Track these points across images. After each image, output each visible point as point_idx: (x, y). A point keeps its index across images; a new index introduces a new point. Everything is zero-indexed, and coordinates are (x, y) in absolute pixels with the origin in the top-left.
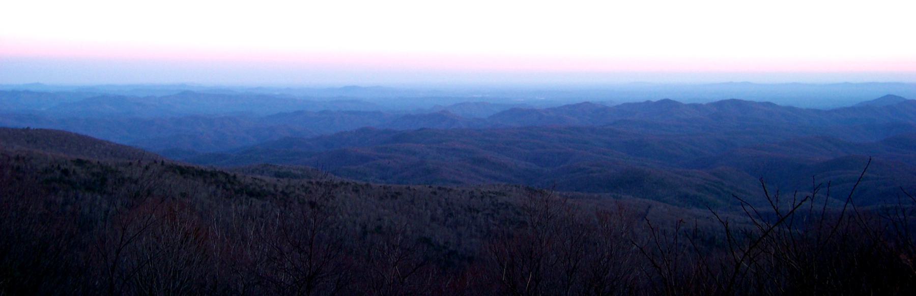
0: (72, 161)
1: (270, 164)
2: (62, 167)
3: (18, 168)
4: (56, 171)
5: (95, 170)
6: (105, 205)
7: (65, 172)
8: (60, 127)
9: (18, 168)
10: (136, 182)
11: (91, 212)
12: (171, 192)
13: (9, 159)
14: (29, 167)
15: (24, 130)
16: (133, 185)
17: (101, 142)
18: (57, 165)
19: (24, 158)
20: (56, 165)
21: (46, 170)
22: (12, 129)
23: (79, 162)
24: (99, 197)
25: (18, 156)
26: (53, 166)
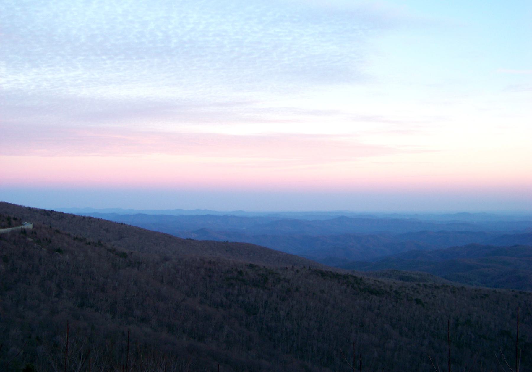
0: (246, 265)
2: (239, 270)
3: (210, 269)
7: (240, 273)
8: (119, 221)
9: (210, 269)
10: (288, 282)
11: (255, 301)
15: (224, 243)
16: (286, 283)
19: (214, 262)
21: (228, 271)
23: (251, 266)
24: (262, 291)
26: (232, 269)
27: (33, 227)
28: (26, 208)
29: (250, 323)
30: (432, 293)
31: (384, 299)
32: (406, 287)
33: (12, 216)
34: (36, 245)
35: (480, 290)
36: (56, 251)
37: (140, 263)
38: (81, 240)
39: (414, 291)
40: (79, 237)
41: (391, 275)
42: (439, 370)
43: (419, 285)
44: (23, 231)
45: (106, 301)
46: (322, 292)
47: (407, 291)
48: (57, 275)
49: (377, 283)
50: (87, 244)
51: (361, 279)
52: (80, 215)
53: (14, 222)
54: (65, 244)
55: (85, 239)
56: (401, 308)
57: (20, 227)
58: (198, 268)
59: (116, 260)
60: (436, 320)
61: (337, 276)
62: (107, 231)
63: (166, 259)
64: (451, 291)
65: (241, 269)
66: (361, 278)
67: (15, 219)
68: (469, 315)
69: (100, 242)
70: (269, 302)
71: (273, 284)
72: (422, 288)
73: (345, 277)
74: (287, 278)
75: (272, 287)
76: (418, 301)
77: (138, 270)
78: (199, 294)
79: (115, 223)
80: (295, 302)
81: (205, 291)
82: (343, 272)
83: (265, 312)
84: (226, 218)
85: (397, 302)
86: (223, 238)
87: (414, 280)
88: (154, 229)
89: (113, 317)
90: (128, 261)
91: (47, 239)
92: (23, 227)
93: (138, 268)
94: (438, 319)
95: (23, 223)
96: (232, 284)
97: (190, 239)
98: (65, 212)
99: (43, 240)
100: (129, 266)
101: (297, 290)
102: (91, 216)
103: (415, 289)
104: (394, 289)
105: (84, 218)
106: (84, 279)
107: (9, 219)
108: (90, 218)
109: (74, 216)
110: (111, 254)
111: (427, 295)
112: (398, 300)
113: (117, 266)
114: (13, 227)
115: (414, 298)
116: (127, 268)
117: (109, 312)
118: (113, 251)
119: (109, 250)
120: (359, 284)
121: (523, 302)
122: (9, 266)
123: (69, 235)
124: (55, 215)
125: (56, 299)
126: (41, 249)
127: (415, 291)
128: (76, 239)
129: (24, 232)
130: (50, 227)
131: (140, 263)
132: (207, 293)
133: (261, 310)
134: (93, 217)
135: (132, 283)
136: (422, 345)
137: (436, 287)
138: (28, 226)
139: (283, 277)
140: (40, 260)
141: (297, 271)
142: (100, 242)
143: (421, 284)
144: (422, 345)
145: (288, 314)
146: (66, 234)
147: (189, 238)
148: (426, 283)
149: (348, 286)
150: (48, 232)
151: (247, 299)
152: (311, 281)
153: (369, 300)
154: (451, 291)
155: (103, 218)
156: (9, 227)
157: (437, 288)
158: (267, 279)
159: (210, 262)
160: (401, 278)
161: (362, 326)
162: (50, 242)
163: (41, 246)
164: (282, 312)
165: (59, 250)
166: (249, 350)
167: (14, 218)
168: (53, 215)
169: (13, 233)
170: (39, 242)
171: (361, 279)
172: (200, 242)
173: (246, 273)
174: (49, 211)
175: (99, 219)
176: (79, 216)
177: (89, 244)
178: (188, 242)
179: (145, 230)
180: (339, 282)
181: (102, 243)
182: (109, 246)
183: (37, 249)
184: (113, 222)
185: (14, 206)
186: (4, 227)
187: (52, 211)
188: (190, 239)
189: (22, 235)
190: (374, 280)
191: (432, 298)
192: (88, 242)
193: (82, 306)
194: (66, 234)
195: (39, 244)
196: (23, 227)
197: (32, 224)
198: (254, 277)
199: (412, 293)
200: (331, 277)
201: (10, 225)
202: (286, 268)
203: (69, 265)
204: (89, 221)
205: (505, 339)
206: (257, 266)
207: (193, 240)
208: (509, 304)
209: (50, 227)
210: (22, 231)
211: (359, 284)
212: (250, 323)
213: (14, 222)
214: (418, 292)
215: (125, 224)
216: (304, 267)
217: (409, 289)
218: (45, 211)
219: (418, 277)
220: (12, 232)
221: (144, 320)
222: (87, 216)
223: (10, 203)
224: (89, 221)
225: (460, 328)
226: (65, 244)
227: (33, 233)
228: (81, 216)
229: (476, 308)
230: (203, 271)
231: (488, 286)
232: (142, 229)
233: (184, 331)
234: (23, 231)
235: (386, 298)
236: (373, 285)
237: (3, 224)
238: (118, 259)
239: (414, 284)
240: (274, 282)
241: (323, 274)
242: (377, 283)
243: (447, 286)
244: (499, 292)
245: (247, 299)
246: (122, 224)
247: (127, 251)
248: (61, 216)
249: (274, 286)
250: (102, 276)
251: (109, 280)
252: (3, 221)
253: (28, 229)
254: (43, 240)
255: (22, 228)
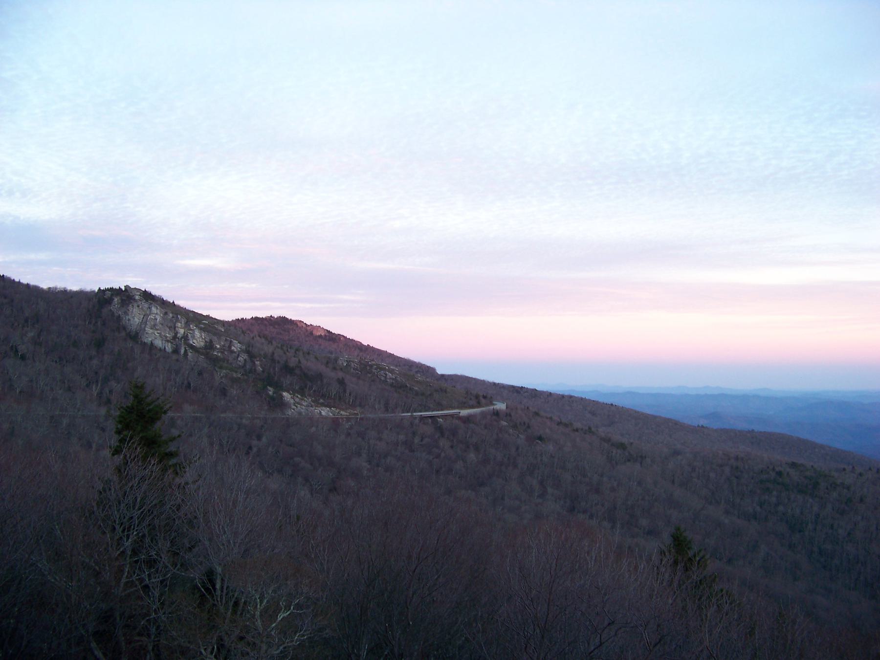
0: (786, 463)
1: (17, 478)
2: (777, 469)
3: (737, 468)
4: (771, 472)
5: (808, 474)
6: (815, 508)
7: (780, 474)
8: (609, 401)
9: (737, 468)
10: (848, 488)
11: (802, 513)
12: (165, 626)
13: (729, 459)
14: (747, 467)
15: (749, 432)
16: (845, 490)
17: (822, 447)
18: (772, 467)
19: (742, 459)
20: (771, 467)
21: (762, 471)
22: (739, 431)
23: (793, 465)
24: (811, 500)
25: (737, 456)
26: (768, 467)
28: (491, 383)
36: (537, 440)
37: (643, 458)
38: (566, 425)
40: (564, 420)
42: (140, 279)
45: (603, 505)
48: (538, 469)
52: (558, 393)
53: (483, 401)
54: (547, 431)
55: (571, 424)
57: (492, 407)
59: (612, 452)
62: (593, 414)
63: (676, 453)
67: (485, 397)
70: (821, 515)
71: (826, 490)
74: (846, 483)
77: (641, 466)
78: (723, 502)
80: (860, 518)
81: (731, 497)
83: (815, 529)
84: (745, 398)
89: (613, 527)
90: (627, 454)
91: (524, 423)
92: (495, 407)
93: (641, 463)
95: (494, 402)
97: (702, 426)
98: (540, 388)
100: (629, 460)
101: (861, 500)
105: (563, 396)
106: (573, 476)
107: (477, 397)
108: (571, 397)
109: (550, 394)
110: (606, 445)
113: (614, 460)
114: (483, 407)
116: (628, 463)
117: (607, 520)
118: (607, 440)
119: (603, 440)
123: (551, 418)
124: (527, 392)
125: (540, 500)
128: (559, 423)
129: (496, 413)
131: (643, 458)
132: (733, 500)
133: (810, 526)
134: (574, 396)
135: (635, 483)
138: (501, 406)
140: (517, 449)
141: (861, 474)
142: (590, 428)
145: (849, 534)
146: (547, 418)
156: (478, 407)
162: (529, 427)
163: (518, 433)
164: (840, 531)
165: (540, 438)
167: (483, 395)
168: (524, 392)
170: (515, 427)
172: (716, 430)
175: (582, 399)
176: (557, 394)
177: (577, 430)
179: (643, 414)
181: (593, 429)
183: (513, 435)
188: (702, 426)
189: (494, 417)
192: (575, 428)
193: (572, 510)
195: (515, 430)
197: (505, 404)
201: (479, 405)
203: (554, 457)
204: (569, 401)
209: (528, 408)
210: (494, 413)
213: (483, 401)
215: (616, 405)
216: (870, 469)
218: (513, 387)
220: (482, 413)
222: (566, 394)
223: (470, 376)
224: (569, 401)
226: (547, 431)
227: (508, 415)
230: (727, 470)
237: (471, 403)
238: (614, 451)
240: (827, 489)
246: (612, 405)
247: (625, 440)
248: (534, 394)
249: (828, 494)
250: (596, 473)
252: (471, 399)
254: (520, 423)
255: (494, 409)
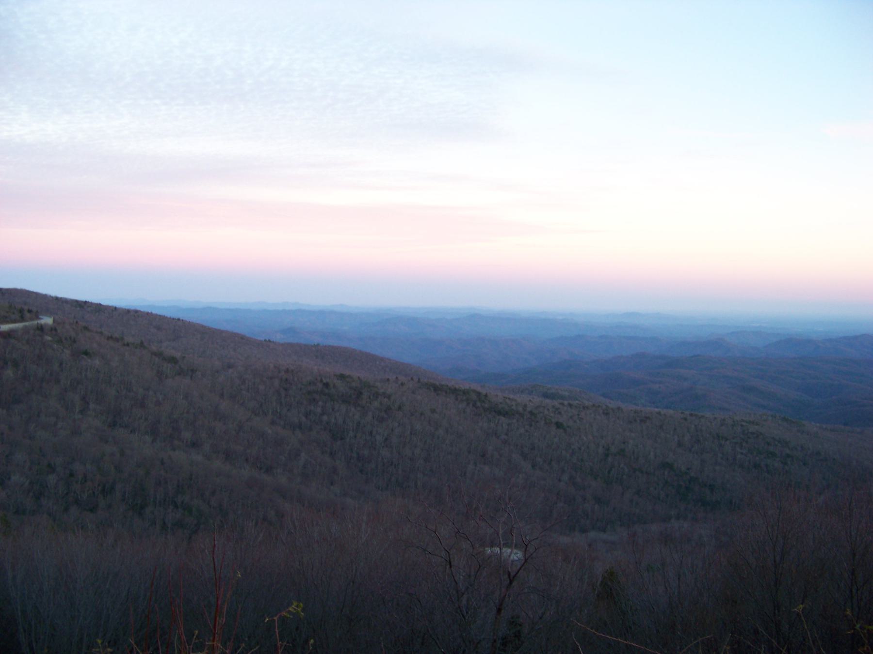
2: (325, 381)
3: (287, 380)
7: (326, 385)
9: (287, 380)
10: (389, 397)
11: (344, 422)
16: (386, 400)
19: (292, 371)
23: (342, 377)
24: (353, 409)
26: (317, 379)
27: (54, 321)
28: (52, 297)
29: (335, 451)
30: (578, 415)
31: (515, 421)
32: (544, 407)
33: (26, 308)
34: (55, 345)
35: (641, 411)
39: (555, 412)
41: (532, 392)
43: (563, 404)
44: (39, 327)
45: (146, 419)
46: (433, 411)
47: (546, 412)
49: (507, 401)
50: (124, 345)
51: (486, 396)
52: (124, 308)
53: (28, 315)
56: (536, 434)
57: (35, 322)
58: (271, 378)
59: (163, 366)
60: (580, 449)
61: (454, 391)
62: (159, 328)
63: (230, 366)
64: (604, 413)
65: (328, 380)
66: (486, 394)
67: (30, 311)
68: (624, 443)
69: (142, 343)
72: (565, 408)
73: (465, 392)
75: (367, 405)
76: (559, 425)
79: (170, 318)
80: (396, 424)
82: (466, 386)
83: (355, 437)
84: (322, 314)
85: (531, 426)
86: (316, 340)
87: (562, 398)
88: (168, 314)
89: (154, 441)
92: (39, 322)
94: (583, 448)
95: (40, 317)
96: (314, 399)
97: (269, 341)
98: (104, 303)
99: (66, 339)
100: (179, 374)
101: (400, 408)
102: (138, 309)
103: (557, 409)
104: (529, 409)
107: (21, 311)
108: (136, 311)
110: (157, 359)
111: (571, 417)
112: (533, 423)
114: (27, 321)
115: (553, 420)
119: (155, 354)
120: (483, 401)
121: (693, 426)
122: (20, 372)
123: (101, 333)
125: (80, 416)
126: (63, 350)
127: (557, 412)
128: (110, 338)
130: (77, 322)
133: (351, 434)
136: (560, 480)
137: (584, 408)
138: (47, 320)
139: (382, 391)
140: (61, 364)
143: (566, 402)
144: (560, 480)
145: (386, 439)
146: (97, 332)
147: (267, 340)
148: (571, 402)
149: (468, 404)
150: (74, 329)
151: (333, 420)
152: (419, 398)
153: (495, 422)
154: (604, 413)
155: (154, 312)
157: (585, 408)
158: (361, 393)
159: (287, 371)
160: (546, 396)
161: (483, 456)
162: (75, 341)
165: (86, 353)
166: (332, 484)
168: (88, 307)
169: (26, 330)
170: (60, 341)
171: (486, 396)
172: (282, 345)
173: (334, 386)
174: (82, 302)
175: (148, 313)
177: (128, 345)
178: (267, 345)
179: (210, 329)
180: (457, 399)
181: (145, 344)
182: (154, 348)
184: (167, 317)
185: (37, 295)
186: (14, 321)
187: (86, 302)
190: (504, 397)
191: (578, 421)
192: (126, 343)
193: (113, 425)
194: (97, 332)
196: (39, 322)
198: (344, 391)
199: (552, 415)
200: (446, 392)
201: (22, 319)
202: (388, 380)
204: (134, 316)
205: (666, 473)
206: (349, 376)
207: (273, 342)
208: (675, 429)
209: (77, 322)
211: (483, 401)
212: (335, 451)
213: (28, 315)
214: (560, 413)
216: (412, 379)
217: (548, 410)
218: (77, 301)
219: (567, 394)
221: (195, 445)
222: (133, 308)
225: (610, 459)
227: (53, 329)
228: (125, 309)
229: (633, 435)
230: (276, 382)
231: (657, 407)
232: (205, 327)
233: (247, 460)
234: (39, 327)
235: (518, 421)
236: (501, 403)
239: (556, 403)
241: (437, 389)
242: (507, 401)
243: (599, 406)
244: (665, 415)
245: (333, 420)
246: (179, 319)
247: (178, 355)
248: (99, 308)
249: (370, 403)
251: (151, 393)
253: (46, 325)
254: (66, 339)
255: (38, 323)
